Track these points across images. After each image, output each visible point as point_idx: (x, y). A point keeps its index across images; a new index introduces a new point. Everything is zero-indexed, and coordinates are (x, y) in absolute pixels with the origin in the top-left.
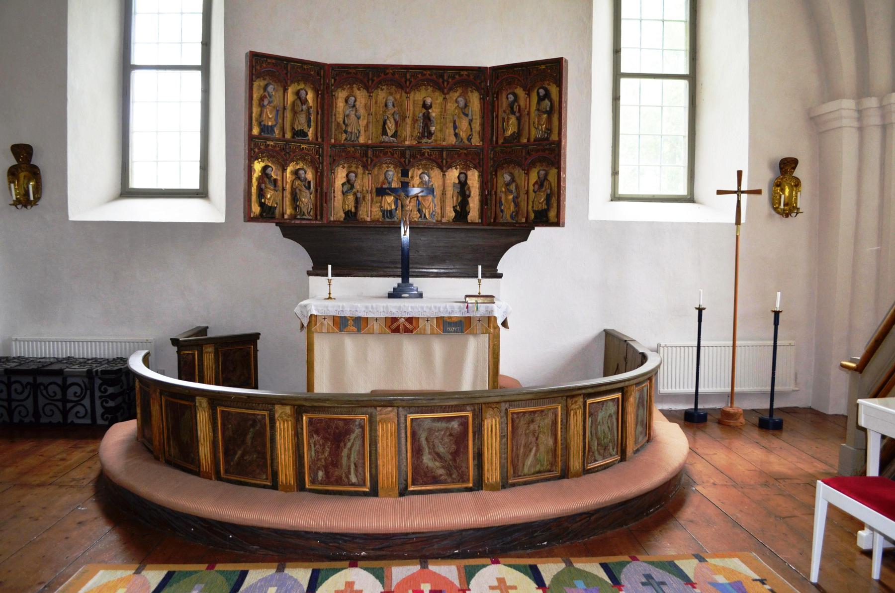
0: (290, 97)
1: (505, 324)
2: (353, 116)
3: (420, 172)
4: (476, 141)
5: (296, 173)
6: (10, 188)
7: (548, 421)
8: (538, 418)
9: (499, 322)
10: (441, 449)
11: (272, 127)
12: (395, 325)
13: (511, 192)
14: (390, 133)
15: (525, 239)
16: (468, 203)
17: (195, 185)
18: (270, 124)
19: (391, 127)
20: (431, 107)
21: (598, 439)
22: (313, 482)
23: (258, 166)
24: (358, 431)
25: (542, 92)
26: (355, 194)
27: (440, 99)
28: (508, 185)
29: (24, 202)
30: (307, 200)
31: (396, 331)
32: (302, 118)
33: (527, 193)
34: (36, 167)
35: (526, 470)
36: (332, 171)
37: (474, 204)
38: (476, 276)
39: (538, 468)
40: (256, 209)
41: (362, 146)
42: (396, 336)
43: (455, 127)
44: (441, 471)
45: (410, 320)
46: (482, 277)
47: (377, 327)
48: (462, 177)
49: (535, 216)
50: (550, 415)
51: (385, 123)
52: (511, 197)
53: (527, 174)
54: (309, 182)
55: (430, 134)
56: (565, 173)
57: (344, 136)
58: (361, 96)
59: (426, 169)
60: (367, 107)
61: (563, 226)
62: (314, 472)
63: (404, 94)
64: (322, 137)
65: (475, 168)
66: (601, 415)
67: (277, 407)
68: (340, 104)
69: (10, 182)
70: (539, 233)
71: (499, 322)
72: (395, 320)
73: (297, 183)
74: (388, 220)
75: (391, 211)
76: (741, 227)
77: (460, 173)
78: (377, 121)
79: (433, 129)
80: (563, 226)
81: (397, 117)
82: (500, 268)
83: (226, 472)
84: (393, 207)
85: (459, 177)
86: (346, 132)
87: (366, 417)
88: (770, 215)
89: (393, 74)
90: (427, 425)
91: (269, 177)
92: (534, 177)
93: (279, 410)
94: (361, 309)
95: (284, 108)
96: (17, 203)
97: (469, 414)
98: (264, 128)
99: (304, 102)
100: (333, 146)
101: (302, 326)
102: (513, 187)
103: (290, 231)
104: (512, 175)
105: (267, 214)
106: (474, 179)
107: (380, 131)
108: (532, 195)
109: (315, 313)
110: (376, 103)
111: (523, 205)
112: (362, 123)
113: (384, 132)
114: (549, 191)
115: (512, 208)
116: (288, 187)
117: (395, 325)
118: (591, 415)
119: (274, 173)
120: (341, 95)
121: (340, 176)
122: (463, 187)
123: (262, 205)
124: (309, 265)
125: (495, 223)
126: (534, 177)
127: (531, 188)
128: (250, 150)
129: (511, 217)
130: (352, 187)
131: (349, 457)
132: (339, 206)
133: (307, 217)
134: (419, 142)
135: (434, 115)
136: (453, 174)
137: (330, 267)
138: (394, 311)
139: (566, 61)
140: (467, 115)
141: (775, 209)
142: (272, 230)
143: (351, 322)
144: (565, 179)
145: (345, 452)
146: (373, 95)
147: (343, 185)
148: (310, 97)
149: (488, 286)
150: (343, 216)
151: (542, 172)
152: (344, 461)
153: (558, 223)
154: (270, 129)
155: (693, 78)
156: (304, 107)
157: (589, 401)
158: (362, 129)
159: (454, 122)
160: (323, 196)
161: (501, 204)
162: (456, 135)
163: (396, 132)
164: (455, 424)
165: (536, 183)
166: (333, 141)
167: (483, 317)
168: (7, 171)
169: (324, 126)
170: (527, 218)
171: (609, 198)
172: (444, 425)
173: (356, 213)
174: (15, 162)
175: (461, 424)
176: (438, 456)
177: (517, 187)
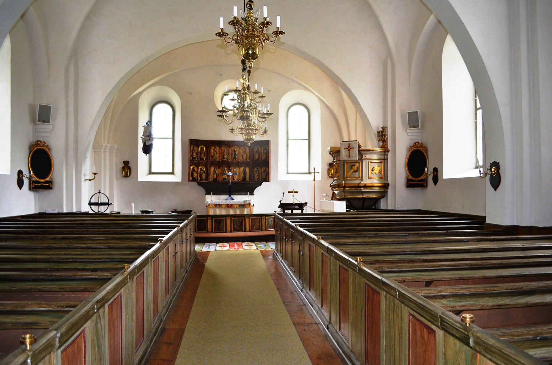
0: (200, 149)
1: (253, 205)
2: (216, 154)
3: (233, 168)
4: (248, 160)
5: (201, 169)
6: (122, 173)
7: (258, 220)
8: (256, 219)
9: (252, 205)
10: (238, 225)
11: (195, 158)
12: (228, 206)
13: (257, 173)
14: (225, 158)
15: (261, 185)
16: (246, 176)
17: (171, 171)
18: (195, 157)
19: (226, 156)
20: (236, 151)
21: (269, 225)
22: (215, 231)
23: (192, 167)
24: (223, 221)
25: (264, 148)
26: (216, 174)
27: (238, 149)
28: (256, 171)
29: (126, 176)
30: (204, 176)
31: (228, 207)
32: (203, 155)
33: (261, 173)
34: (129, 167)
35: (254, 229)
36: (210, 168)
37: (248, 176)
38: (211, 195)
39: (256, 229)
40: (191, 178)
41: (218, 162)
42: (228, 209)
43: (242, 156)
44: (238, 229)
45: (231, 204)
46: (213, 195)
47: (224, 206)
48: (244, 169)
49: (263, 180)
50: (259, 219)
51: (224, 155)
52: (257, 175)
53: (261, 169)
54: (204, 171)
55: (236, 158)
56: (270, 168)
57: (213, 159)
58: (218, 149)
59: (235, 167)
60: (219, 151)
61: (270, 182)
62: (215, 229)
63: (229, 148)
64: (208, 159)
65: (248, 167)
66: (269, 220)
67: (208, 217)
68: (212, 150)
69: (122, 171)
70: (264, 184)
71: (252, 205)
72: (228, 204)
73: (201, 171)
74: (225, 181)
75: (226, 178)
76: (315, 181)
77: (244, 168)
78: (222, 155)
79: (237, 157)
80: (270, 182)
81: (227, 154)
82: (254, 193)
83: (197, 231)
84: (226, 177)
85: (243, 169)
86: (214, 158)
87: (224, 219)
88: (328, 178)
89: (226, 143)
90: (236, 220)
91: (194, 170)
92: (263, 169)
93: (209, 218)
94: (220, 202)
95: (198, 152)
96: (124, 177)
97: (243, 218)
98: (193, 158)
99: (203, 150)
100: (210, 162)
101: (206, 206)
102: (257, 172)
103: (200, 184)
104: (257, 169)
105: (194, 180)
106: (247, 170)
107: (223, 157)
108: (262, 174)
109: (210, 203)
110: (222, 150)
111: (260, 176)
112: (218, 155)
113: (224, 158)
114: (266, 173)
115: (257, 178)
116: (199, 172)
117: (228, 206)
118: (267, 220)
119: (196, 169)
120: (213, 148)
121: (212, 169)
122: (245, 171)
123: (193, 177)
124: (205, 192)
125: (253, 181)
126: (263, 169)
127: (262, 172)
128: (190, 163)
129: (257, 180)
130: (216, 172)
131: (221, 226)
132: (212, 177)
133: (204, 180)
134: (233, 161)
135: (237, 153)
136: (242, 169)
137: (212, 193)
138: (228, 202)
139: (270, 141)
140: (245, 153)
141: (329, 176)
142: (195, 184)
143: (218, 205)
144: (270, 170)
145: (221, 225)
146: (221, 148)
147: (213, 172)
148: (204, 149)
149: (250, 197)
150: (213, 180)
151: (265, 168)
152: (221, 227)
153: (268, 181)
154: (195, 158)
155: (309, 140)
156: (203, 152)
157: (266, 217)
158: (218, 157)
159: (242, 155)
160: (207, 174)
161: (254, 176)
162: (243, 158)
163: (227, 158)
164: (240, 220)
165: (263, 171)
166: (210, 160)
167: (248, 204)
168: (121, 168)
169: (208, 157)
170: (261, 180)
171: (286, 173)
172: (239, 220)
173: (216, 179)
174: (124, 165)
175: (241, 220)
176: (237, 226)
177: (259, 172)
